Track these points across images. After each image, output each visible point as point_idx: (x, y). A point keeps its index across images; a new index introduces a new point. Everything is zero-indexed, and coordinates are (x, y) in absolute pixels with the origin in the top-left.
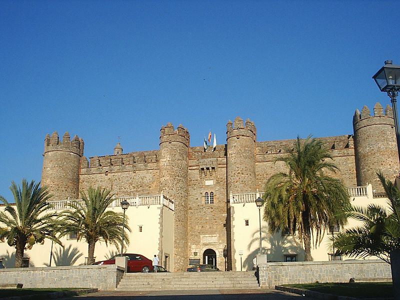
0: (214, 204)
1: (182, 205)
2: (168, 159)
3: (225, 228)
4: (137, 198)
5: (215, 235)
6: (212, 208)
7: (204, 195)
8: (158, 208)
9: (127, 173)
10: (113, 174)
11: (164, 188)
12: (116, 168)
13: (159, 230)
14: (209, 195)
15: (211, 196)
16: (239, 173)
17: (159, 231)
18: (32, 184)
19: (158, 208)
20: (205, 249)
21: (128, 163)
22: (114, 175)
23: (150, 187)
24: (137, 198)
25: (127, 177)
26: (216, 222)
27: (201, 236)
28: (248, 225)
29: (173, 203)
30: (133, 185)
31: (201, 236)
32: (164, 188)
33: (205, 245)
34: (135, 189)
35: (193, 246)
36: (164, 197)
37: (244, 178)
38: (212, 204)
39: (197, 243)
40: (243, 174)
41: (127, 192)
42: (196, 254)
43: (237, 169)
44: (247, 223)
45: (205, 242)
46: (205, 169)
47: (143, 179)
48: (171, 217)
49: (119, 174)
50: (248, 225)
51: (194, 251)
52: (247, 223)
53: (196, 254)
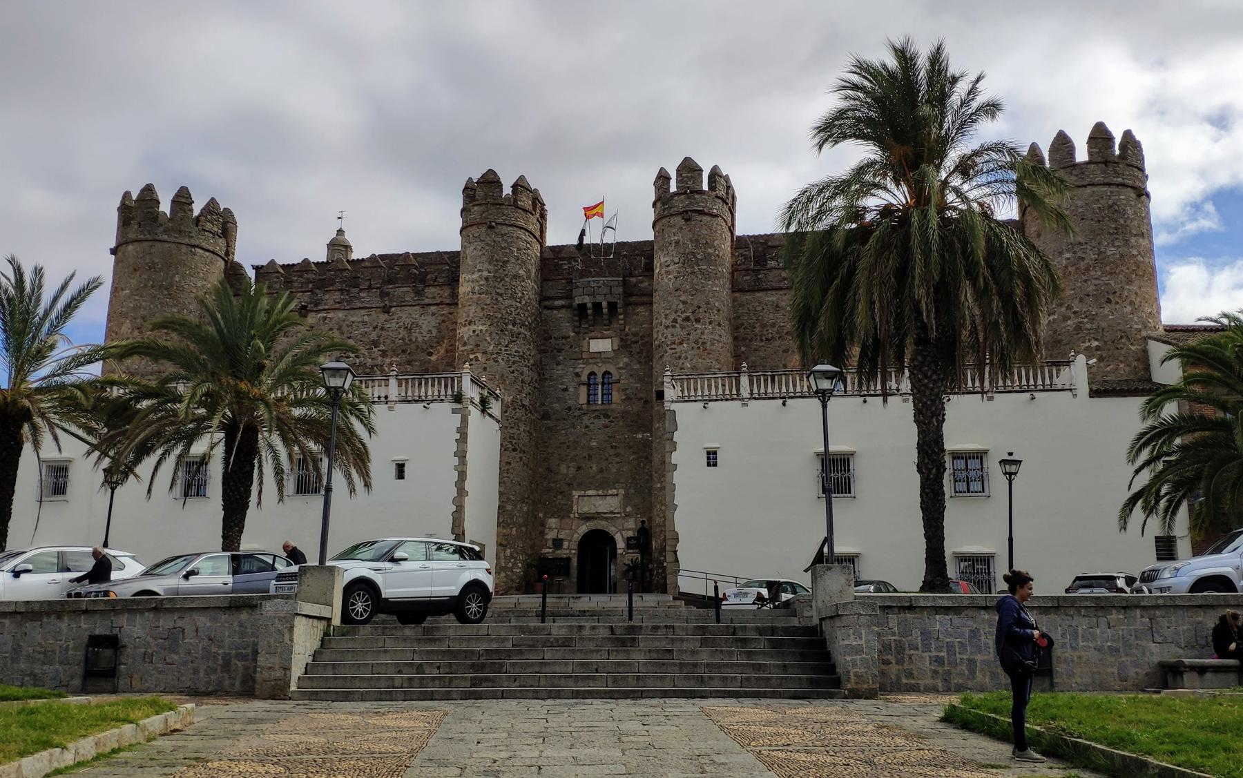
0: (614, 406)
1: (523, 406)
2: (485, 274)
4: (393, 382)
5: (615, 492)
6: (606, 416)
7: (584, 378)
10: (323, 315)
12: (331, 298)
14: (599, 380)
15: (603, 384)
16: (687, 319)
17: (455, 476)
19: (454, 411)
20: (584, 529)
22: (325, 318)
23: (430, 354)
24: (393, 382)
25: (364, 323)
26: (617, 455)
27: (576, 494)
28: (715, 465)
31: (576, 494)
33: (586, 518)
35: (552, 522)
36: (474, 381)
37: (702, 333)
38: (606, 407)
39: (564, 512)
40: (698, 321)
42: (558, 543)
43: (681, 306)
45: (586, 509)
46: (692, 318)
47: (409, 330)
48: (485, 435)
49: (341, 314)
50: (715, 465)
51: (551, 535)
53: (558, 543)
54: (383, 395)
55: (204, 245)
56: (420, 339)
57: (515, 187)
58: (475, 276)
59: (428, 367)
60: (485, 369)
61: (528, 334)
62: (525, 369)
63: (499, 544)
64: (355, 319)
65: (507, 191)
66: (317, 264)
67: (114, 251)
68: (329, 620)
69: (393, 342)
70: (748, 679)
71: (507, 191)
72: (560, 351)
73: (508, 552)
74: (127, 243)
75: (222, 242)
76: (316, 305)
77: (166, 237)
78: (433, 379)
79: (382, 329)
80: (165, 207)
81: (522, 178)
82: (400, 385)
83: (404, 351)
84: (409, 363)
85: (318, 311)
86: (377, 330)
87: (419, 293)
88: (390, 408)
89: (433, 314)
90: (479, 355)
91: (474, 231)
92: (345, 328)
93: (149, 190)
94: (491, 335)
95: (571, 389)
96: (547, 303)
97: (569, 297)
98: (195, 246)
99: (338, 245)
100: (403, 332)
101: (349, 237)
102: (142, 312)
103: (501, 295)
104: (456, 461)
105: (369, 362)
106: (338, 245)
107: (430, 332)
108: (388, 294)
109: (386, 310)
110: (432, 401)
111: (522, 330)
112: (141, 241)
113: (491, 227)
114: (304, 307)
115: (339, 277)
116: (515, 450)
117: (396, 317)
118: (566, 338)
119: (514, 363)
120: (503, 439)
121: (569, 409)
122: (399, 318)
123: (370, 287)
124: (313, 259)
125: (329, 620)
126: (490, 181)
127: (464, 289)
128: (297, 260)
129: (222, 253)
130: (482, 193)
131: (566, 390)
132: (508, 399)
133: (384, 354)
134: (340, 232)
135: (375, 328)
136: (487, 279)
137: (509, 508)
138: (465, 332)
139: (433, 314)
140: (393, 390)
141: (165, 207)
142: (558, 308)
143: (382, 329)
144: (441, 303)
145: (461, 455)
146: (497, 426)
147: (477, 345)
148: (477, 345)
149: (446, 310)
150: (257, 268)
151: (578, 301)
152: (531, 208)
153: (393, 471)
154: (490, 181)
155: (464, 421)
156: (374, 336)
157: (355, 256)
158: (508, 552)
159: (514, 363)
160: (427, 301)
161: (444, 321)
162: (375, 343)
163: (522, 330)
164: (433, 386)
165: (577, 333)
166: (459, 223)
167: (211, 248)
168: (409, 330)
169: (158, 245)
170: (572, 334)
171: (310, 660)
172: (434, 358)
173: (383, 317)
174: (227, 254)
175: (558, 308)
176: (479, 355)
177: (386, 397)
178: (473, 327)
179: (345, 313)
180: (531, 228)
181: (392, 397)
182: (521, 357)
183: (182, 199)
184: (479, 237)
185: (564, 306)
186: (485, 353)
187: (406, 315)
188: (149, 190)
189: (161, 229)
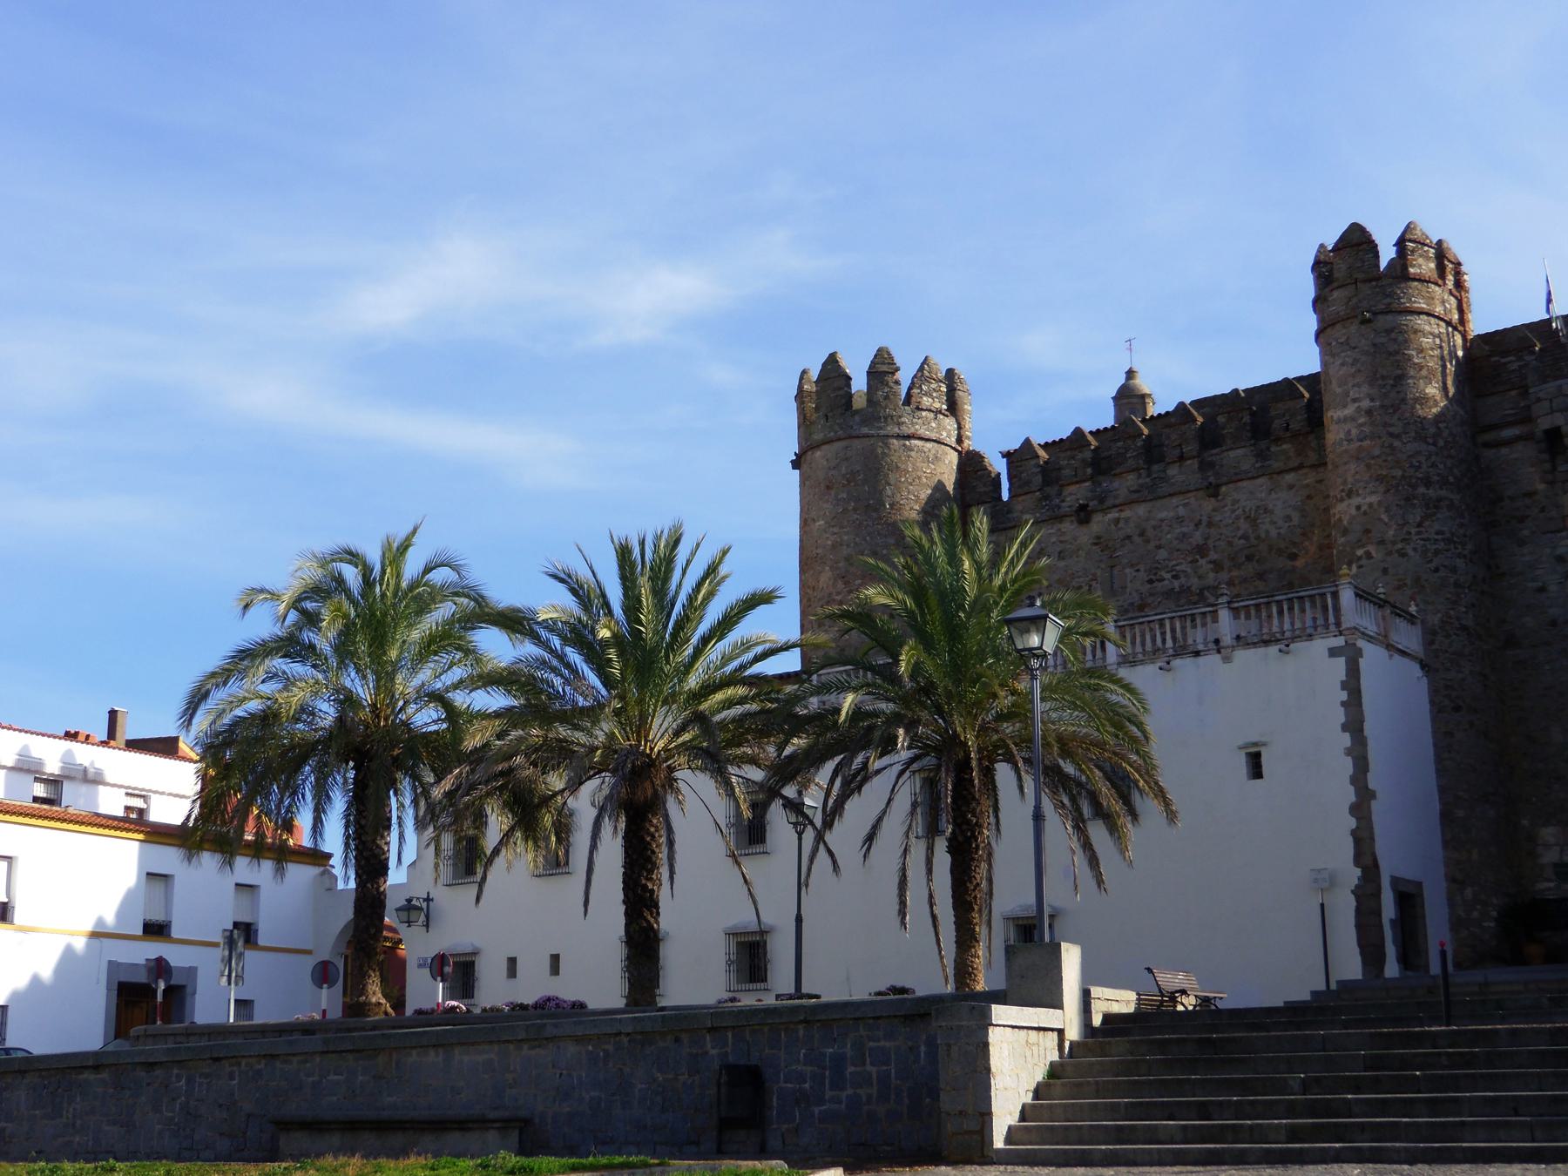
1: (1464, 628)
2: (1366, 404)
3: (750, 525)
4: (1224, 614)
8: (1333, 652)
9: (1175, 500)
10: (1113, 515)
11: (1360, 552)
12: (1125, 484)
13: (1349, 762)
17: (1347, 765)
18: (642, 543)
19: (1333, 652)
21: (1177, 452)
22: (1117, 521)
23: (1293, 557)
24: (1224, 614)
25: (1180, 520)
29: (1411, 619)
30: (1213, 556)
32: (1360, 552)
34: (1224, 576)
36: (1361, 595)
41: (1185, 590)
44: (1255, 767)
47: (1253, 521)
48: (1395, 686)
49: (1141, 510)
52: (1255, 767)
54: (1211, 638)
55: (922, 432)
56: (1274, 533)
57: (1401, 243)
58: (1350, 410)
59: (1277, 588)
60: (1385, 571)
61: (1456, 497)
62: (1460, 563)
63: (1451, 879)
64: (1163, 515)
65: (1387, 254)
66: (1096, 433)
67: (796, 464)
68: (1061, 1032)
69: (1230, 544)
70: (1317, 1080)
71: (1387, 254)
72: (1522, 520)
73: (1469, 892)
74: (817, 446)
75: (950, 423)
76: (1102, 501)
77: (865, 430)
78: (1290, 600)
79: (1210, 524)
80: (859, 384)
81: (1409, 228)
82: (1236, 617)
83: (1249, 558)
84: (1261, 576)
85: (1105, 511)
86: (1202, 528)
87: (1262, 456)
88: (1227, 660)
89: (1291, 487)
90: (1371, 549)
91: (1339, 333)
92: (1150, 533)
93: (832, 362)
94: (1387, 510)
95: (1553, 588)
96: (1488, 437)
97: (1527, 419)
98: (909, 437)
99: (1129, 398)
100: (1244, 526)
101: (1143, 384)
102: (845, 551)
103: (1398, 436)
104: (1346, 740)
105: (1195, 583)
106: (1129, 398)
107: (1288, 518)
108: (1212, 465)
109: (1213, 491)
110: (1294, 639)
111: (1443, 493)
112: (830, 441)
113: (1365, 322)
114: (1083, 508)
115: (1141, 449)
116: (1457, 709)
117: (1229, 500)
118: (1530, 494)
119: (1437, 552)
120: (1434, 692)
121: (1554, 623)
122: (1235, 502)
123: (1182, 458)
124: (1088, 427)
125: (1061, 1032)
126: (1357, 241)
127: (1334, 434)
128: (1065, 433)
129: (953, 441)
130: (1343, 267)
131: (1542, 590)
132: (1434, 620)
133: (1217, 566)
134: (1130, 374)
135: (1197, 525)
136: (1369, 412)
137: (1461, 813)
138: (1344, 510)
139: (1291, 487)
140: (1226, 624)
141: (859, 384)
142: (1509, 442)
143: (1210, 524)
144: (1301, 467)
145: (1354, 725)
146: (1416, 670)
147: (1368, 531)
148: (1368, 531)
149: (1310, 478)
150: (1007, 455)
151: (1545, 423)
152: (1435, 276)
153: (1241, 764)
154: (1357, 241)
155: (1353, 671)
156: (1197, 538)
157: (1153, 410)
158: (1469, 892)
159: (1437, 552)
160: (1277, 465)
161: (1309, 497)
162: (1202, 550)
163: (1443, 493)
164: (1303, 611)
165: (1552, 483)
166: (1311, 322)
167: (933, 436)
168: (1253, 521)
169: (857, 443)
170: (1541, 487)
171: (1028, 1099)
172: (1299, 563)
173: (1209, 505)
174: (960, 440)
175: (1509, 442)
176: (1371, 549)
177: (1217, 641)
178: (1356, 501)
179: (1149, 505)
180: (1439, 310)
181: (1227, 640)
182: (1448, 541)
183: (881, 369)
184: (1347, 343)
185: (1518, 439)
186: (1382, 542)
187: (1245, 495)
188: (832, 362)
189: (857, 418)
